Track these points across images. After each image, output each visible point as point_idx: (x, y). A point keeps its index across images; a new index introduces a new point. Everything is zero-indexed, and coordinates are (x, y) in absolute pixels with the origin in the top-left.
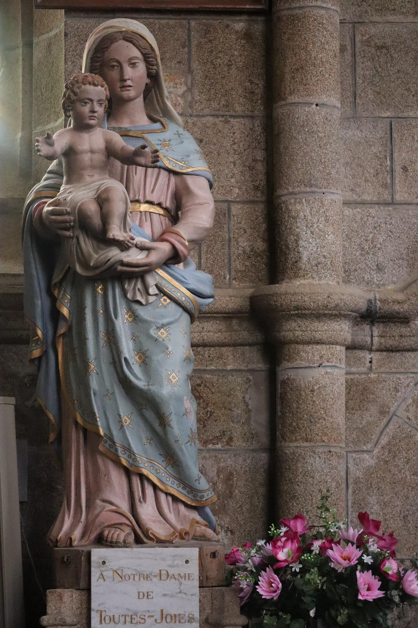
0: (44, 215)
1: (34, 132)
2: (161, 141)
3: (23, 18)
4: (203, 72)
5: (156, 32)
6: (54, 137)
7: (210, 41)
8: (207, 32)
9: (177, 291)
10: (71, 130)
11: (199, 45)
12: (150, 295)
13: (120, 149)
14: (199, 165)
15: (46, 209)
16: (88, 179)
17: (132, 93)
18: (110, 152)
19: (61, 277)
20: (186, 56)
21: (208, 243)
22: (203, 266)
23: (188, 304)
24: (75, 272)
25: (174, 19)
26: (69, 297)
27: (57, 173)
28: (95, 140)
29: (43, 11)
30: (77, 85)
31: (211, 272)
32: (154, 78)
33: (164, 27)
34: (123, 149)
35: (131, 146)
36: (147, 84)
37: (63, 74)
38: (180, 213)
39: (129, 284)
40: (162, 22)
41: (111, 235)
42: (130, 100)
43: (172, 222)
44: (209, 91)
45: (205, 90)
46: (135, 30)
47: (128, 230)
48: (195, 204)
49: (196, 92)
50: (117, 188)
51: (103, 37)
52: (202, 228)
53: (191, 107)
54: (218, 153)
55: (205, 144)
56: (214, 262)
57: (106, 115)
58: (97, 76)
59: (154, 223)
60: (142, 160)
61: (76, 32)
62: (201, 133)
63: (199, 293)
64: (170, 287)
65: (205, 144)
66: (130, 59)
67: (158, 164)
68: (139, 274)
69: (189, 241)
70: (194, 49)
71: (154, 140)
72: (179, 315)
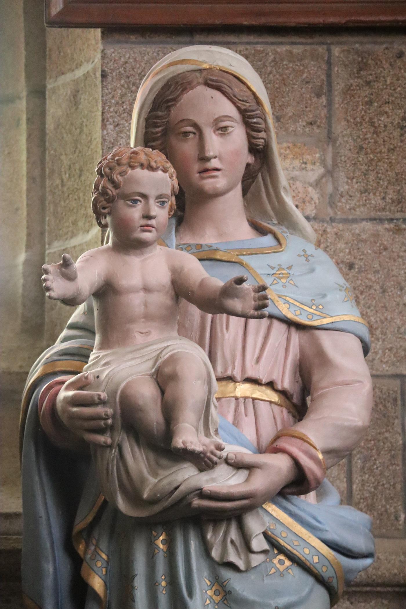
0: (59, 405)
1: (47, 252)
2: (273, 268)
3: (27, 44)
4: (355, 140)
5: (269, 69)
6: (77, 264)
7: (368, 83)
8: (362, 66)
9: (302, 544)
10: (107, 250)
11: (348, 91)
12: (253, 552)
13: (197, 284)
14: (343, 311)
15: (64, 394)
16: (139, 339)
17: (219, 182)
18: (181, 291)
19: (90, 519)
20: (324, 113)
21: (366, 453)
22: (356, 496)
23: (324, 569)
24: (116, 511)
25: (302, 44)
26: (104, 556)
27: (84, 328)
28: (151, 269)
29: (64, 31)
30: (118, 169)
31: (370, 508)
32: (261, 154)
33: (282, 60)
34: (202, 284)
35: (217, 279)
36: (248, 165)
37: (100, 146)
38: (308, 399)
39: (215, 531)
40: (279, 50)
41: (179, 442)
42: (217, 194)
43: (293, 416)
44: (365, 175)
45: (358, 173)
46: (226, 66)
47: (212, 432)
48: (337, 384)
49: (341, 176)
50: (192, 356)
51: (169, 81)
52: (349, 428)
53: (332, 204)
54: (382, 288)
55: (360, 272)
56: (375, 488)
57: (174, 221)
58: (155, 151)
59: (260, 419)
60: (236, 304)
61: (122, 70)
62: (350, 252)
63: (345, 548)
64: (291, 537)
65: (360, 272)
66: (217, 121)
67: (266, 311)
68: (233, 513)
69: (326, 452)
70: (337, 99)
71: (260, 267)
72: (307, 590)
